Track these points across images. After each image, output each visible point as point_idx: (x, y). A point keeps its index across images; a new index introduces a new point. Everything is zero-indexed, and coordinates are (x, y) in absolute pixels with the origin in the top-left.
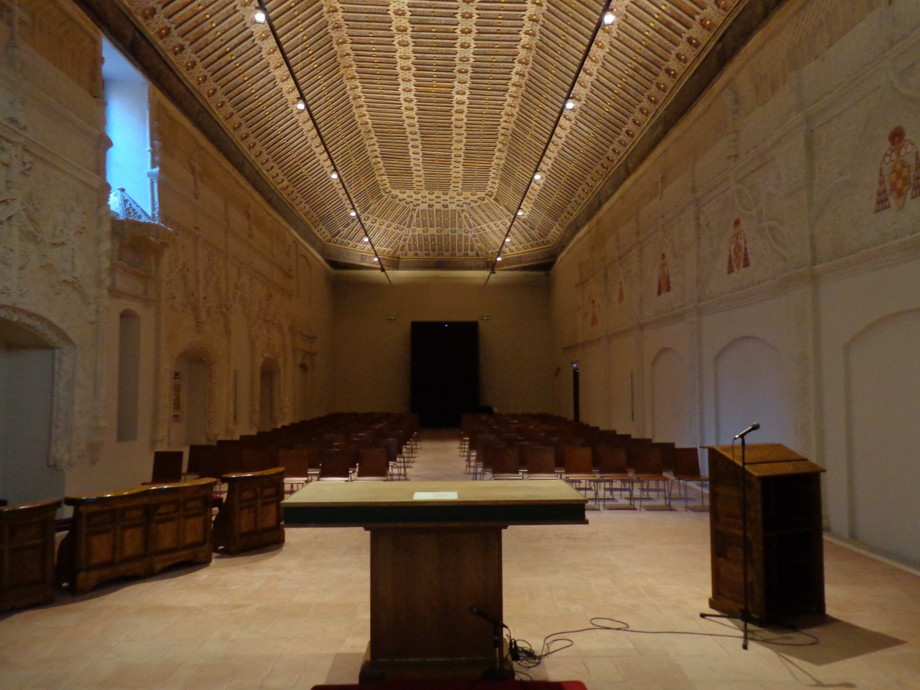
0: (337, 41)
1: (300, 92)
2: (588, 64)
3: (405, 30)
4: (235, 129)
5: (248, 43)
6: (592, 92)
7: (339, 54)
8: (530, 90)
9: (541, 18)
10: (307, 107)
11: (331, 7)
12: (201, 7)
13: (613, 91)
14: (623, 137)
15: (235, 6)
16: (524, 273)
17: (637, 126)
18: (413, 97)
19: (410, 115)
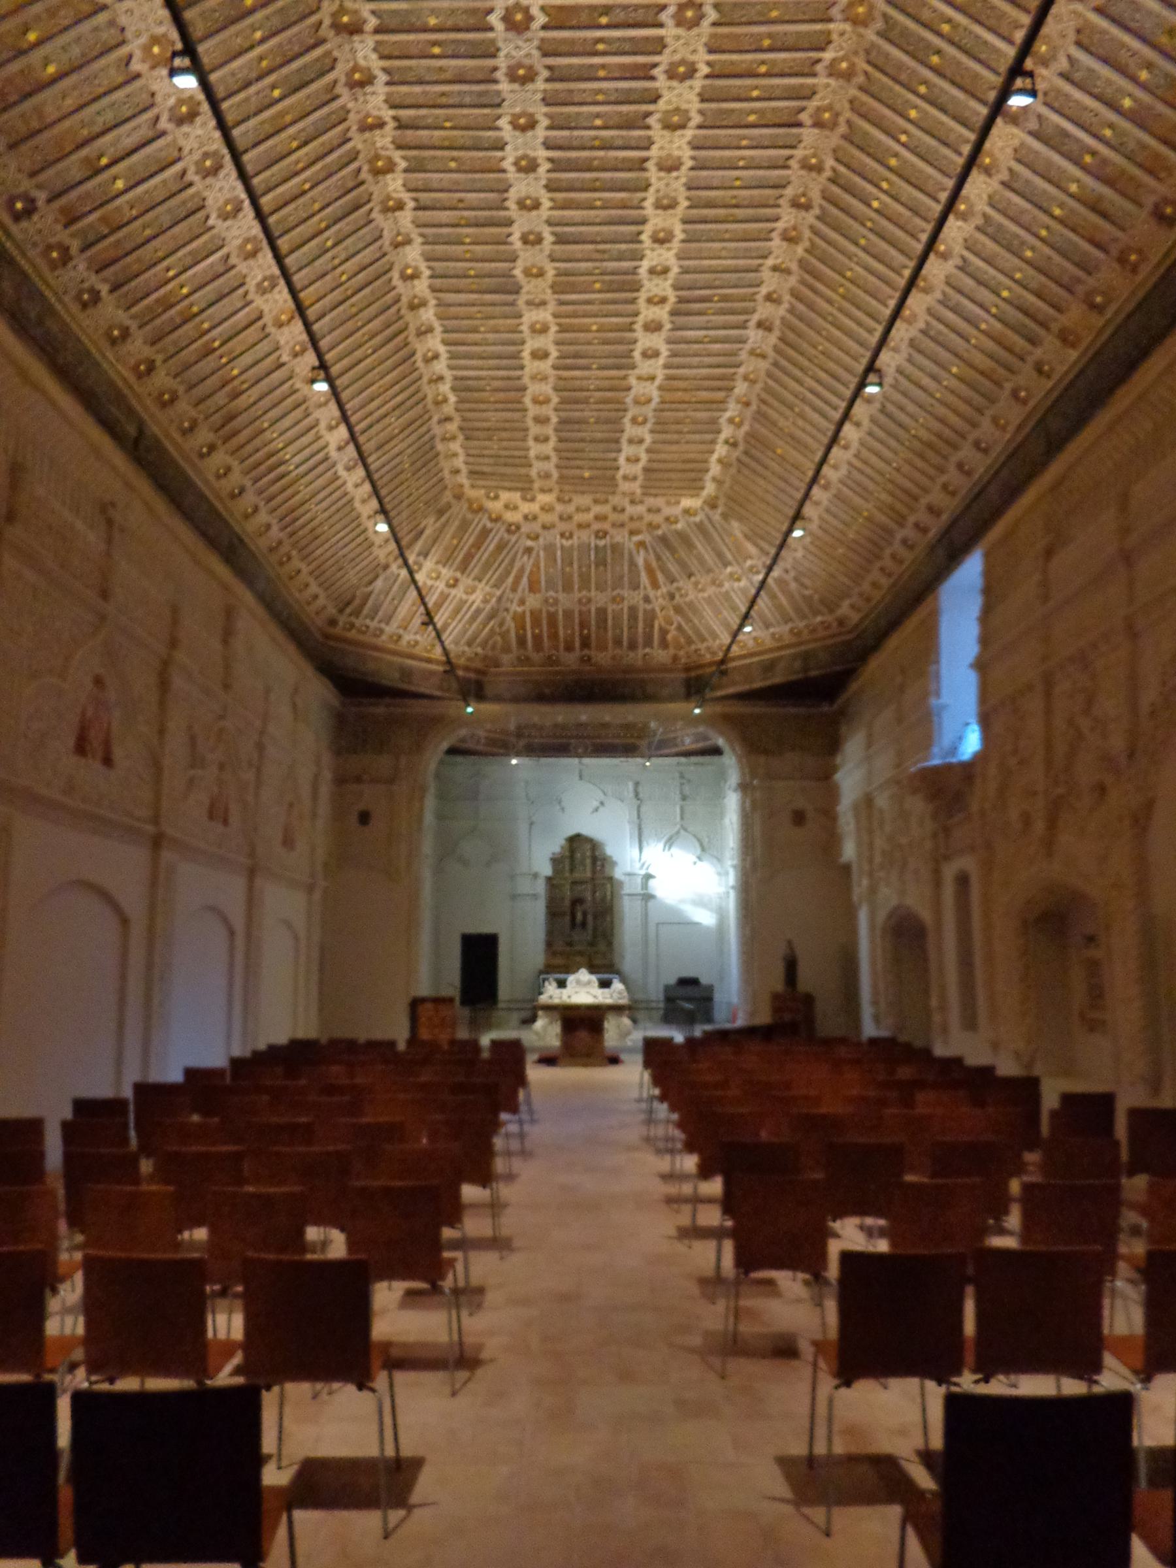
0: (425, 355)
1: (320, 355)
2: (816, 492)
3: (536, 206)
4: (185, 432)
5: (251, 334)
6: (870, 434)
7: (404, 300)
8: (784, 363)
9: (830, 162)
10: (335, 392)
11: (356, 68)
12: (171, 273)
13: (932, 396)
14: (887, 562)
15: (228, 256)
16: (1020, 316)
17: (1002, 425)
18: (550, 318)
19: (539, 379)
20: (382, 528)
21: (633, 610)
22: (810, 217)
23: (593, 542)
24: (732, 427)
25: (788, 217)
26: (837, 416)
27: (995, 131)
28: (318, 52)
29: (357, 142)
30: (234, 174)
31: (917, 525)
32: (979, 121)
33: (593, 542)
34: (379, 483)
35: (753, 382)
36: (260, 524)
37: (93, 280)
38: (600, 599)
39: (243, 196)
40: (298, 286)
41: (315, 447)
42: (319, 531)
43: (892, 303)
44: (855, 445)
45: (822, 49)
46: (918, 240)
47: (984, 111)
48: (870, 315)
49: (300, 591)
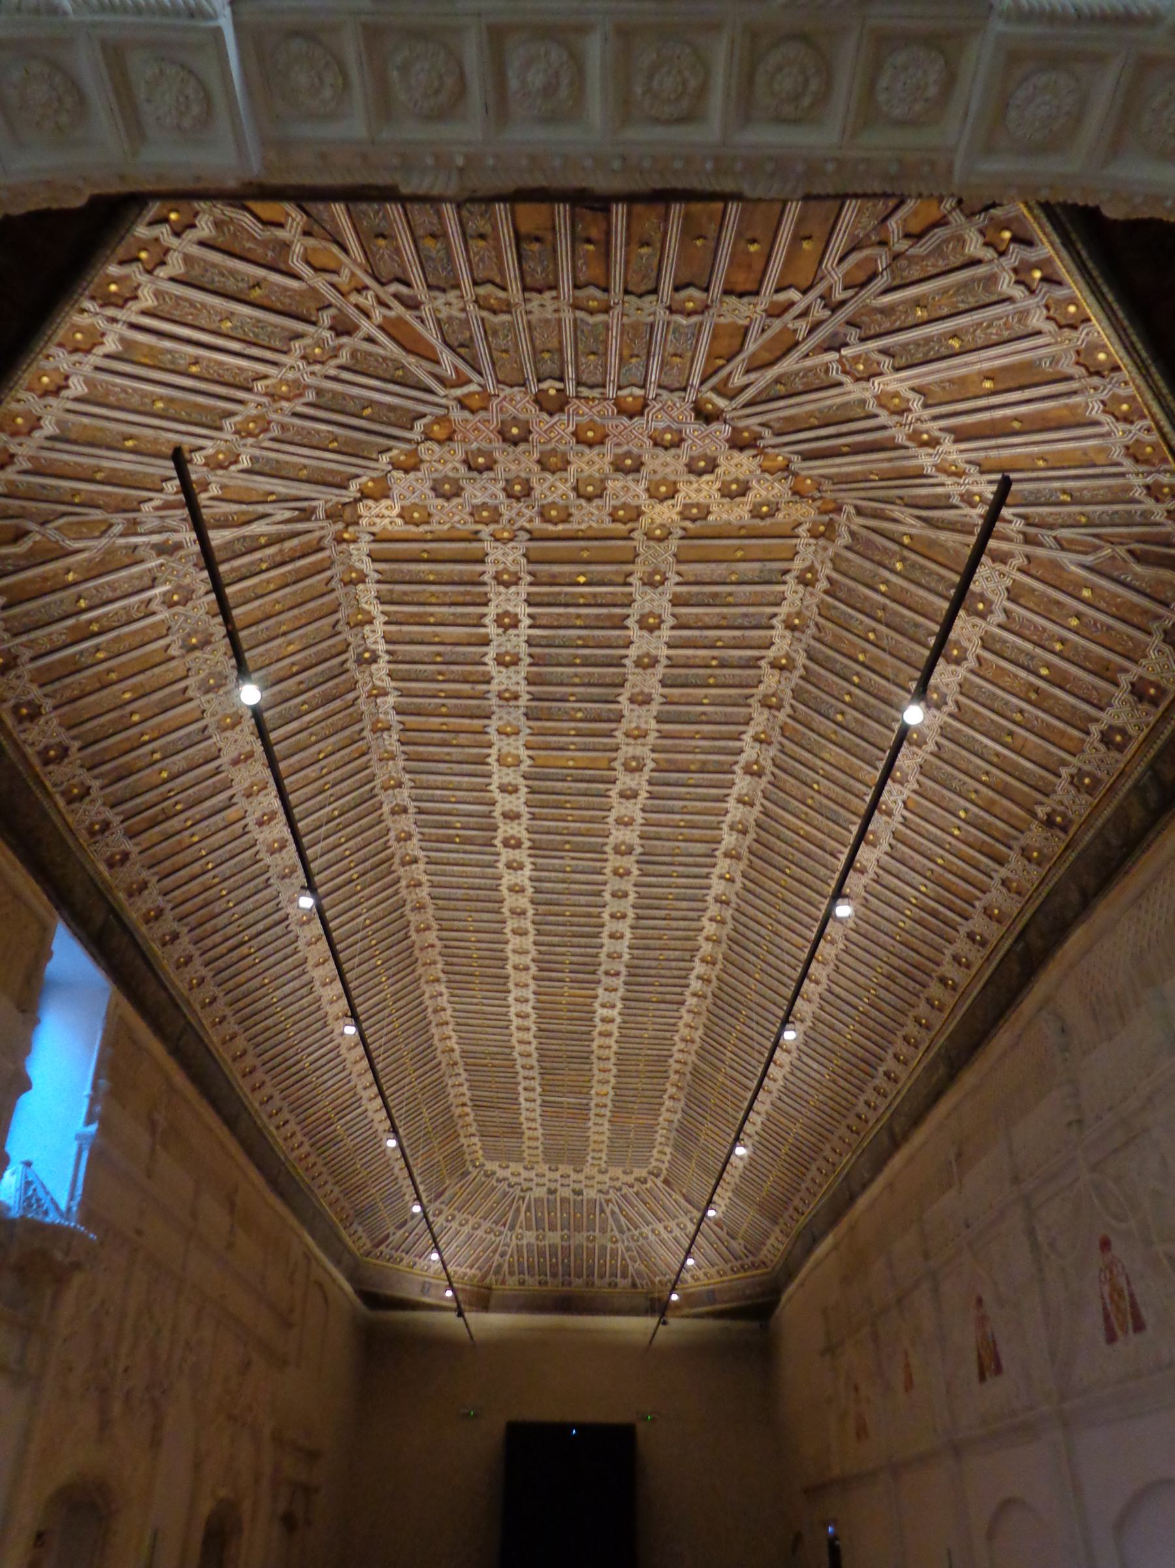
10: (361, 1032)
13: (856, 1008)
20: (350, 1030)
21: (603, 1248)
22: (773, 751)
23: (572, 1197)
24: (735, 834)
25: (771, 680)
26: (789, 993)
27: (958, 623)
28: (320, 556)
29: (348, 635)
30: (274, 793)
31: (887, 1074)
32: (922, 664)
33: (572, 1197)
34: (381, 1074)
35: (744, 832)
36: (287, 1137)
37: (109, 814)
38: (580, 1238)
39: (290, 837)
40: (288, 789)
41: (276, 917)
42: (217, 907)
43: (855, 829)
44: (872, 868)
45: (778, 604)
46: (876, 768)
47: (946, 605)
48: (818, 893)
49: (111, 865)
